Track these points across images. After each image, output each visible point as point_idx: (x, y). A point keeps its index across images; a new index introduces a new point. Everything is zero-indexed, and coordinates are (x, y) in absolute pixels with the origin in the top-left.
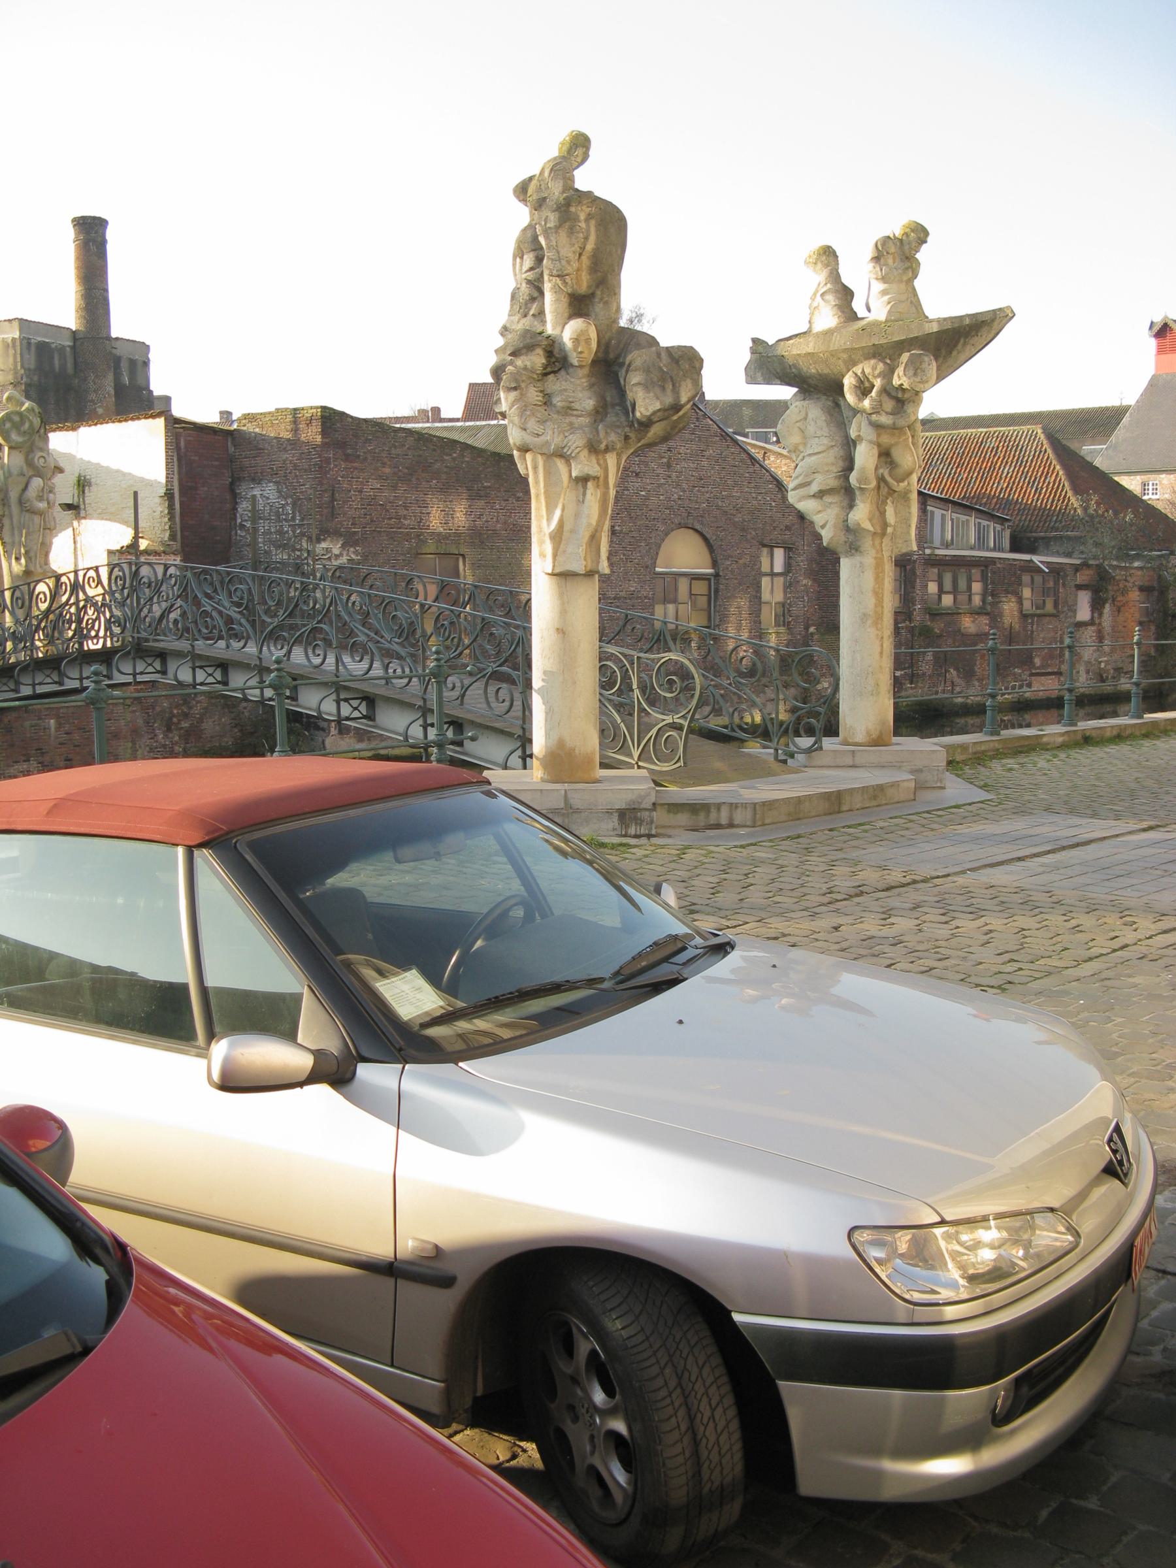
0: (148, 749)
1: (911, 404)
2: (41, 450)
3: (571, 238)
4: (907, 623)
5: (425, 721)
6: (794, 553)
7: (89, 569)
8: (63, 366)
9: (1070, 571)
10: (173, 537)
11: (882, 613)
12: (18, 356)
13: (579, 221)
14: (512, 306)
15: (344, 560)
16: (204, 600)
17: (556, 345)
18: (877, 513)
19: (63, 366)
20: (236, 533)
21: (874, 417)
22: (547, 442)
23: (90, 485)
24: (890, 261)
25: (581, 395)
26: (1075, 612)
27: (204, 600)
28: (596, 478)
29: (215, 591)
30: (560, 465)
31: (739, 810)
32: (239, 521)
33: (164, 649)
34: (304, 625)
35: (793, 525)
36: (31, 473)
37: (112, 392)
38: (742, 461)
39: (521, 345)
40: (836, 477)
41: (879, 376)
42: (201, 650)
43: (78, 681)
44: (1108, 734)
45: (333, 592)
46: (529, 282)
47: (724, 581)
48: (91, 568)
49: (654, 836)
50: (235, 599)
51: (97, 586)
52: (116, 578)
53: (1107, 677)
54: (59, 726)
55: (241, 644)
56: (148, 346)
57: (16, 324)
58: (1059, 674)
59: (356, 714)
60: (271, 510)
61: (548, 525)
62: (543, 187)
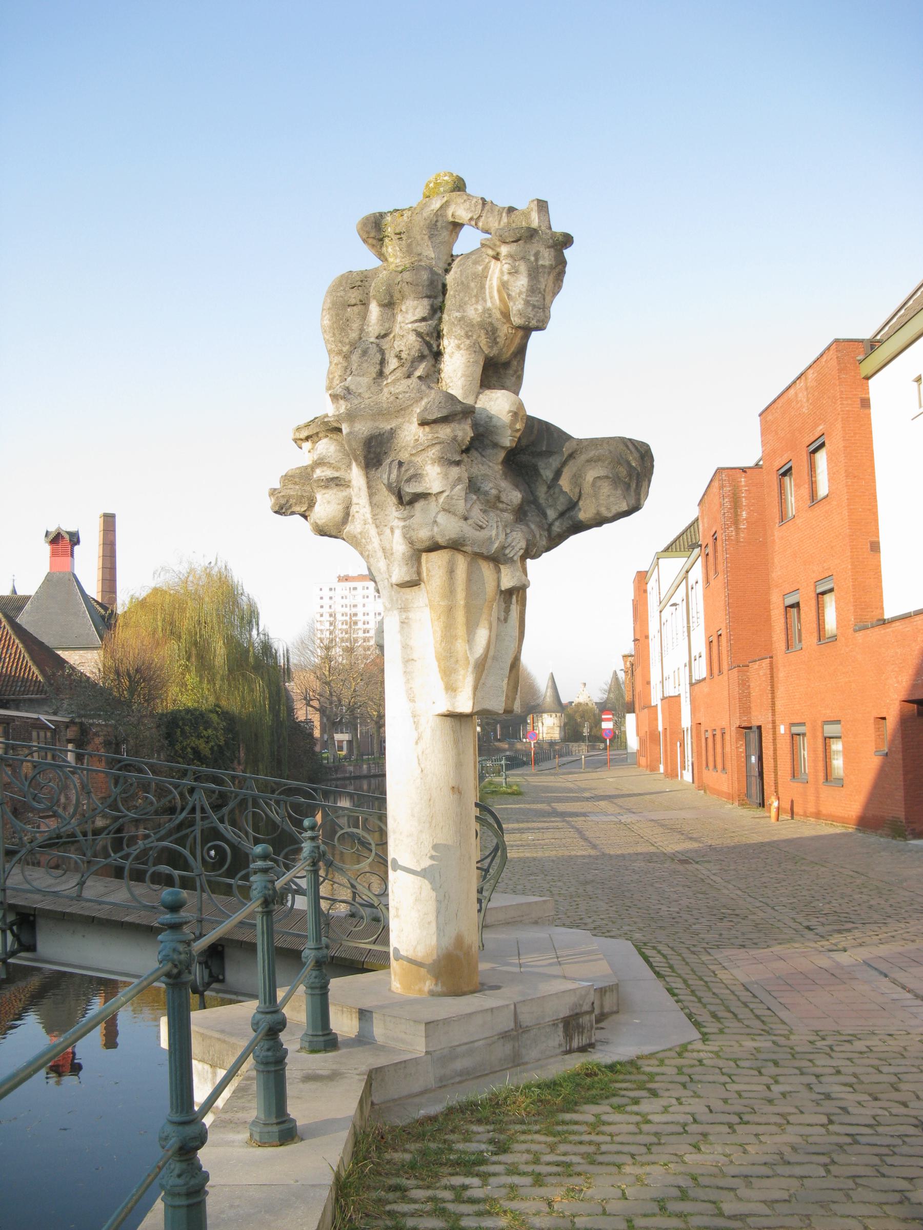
22: (490, 538)
30: (487, 569)
31: (608, 994)
46: (419, 334)
62: (439, 224)
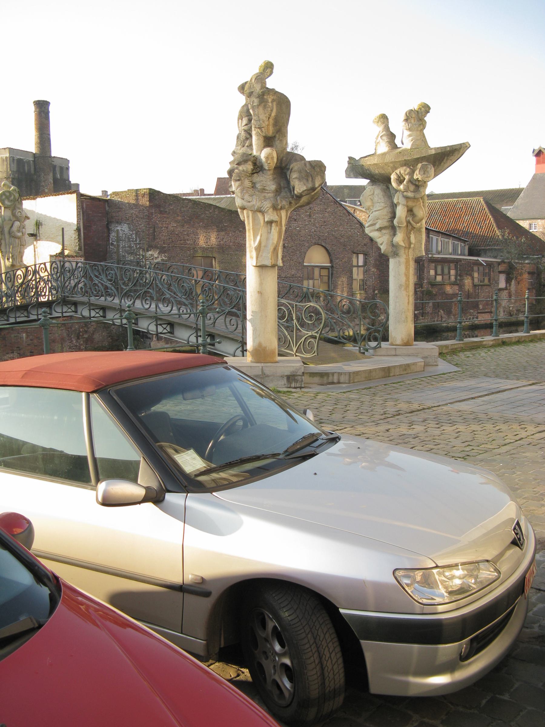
0: (68, 347)
1: (422, 187)
2: (19, 208)
3: (264, 110)
4: (421, 289)
5: (197, 334)
6: (368, 256)
7: (41, 264)
8: (29, 170)
9: (496, 265)
10: (80, 249)
11: (409, 284)
12: (9, 165)
13: (268, 103)
14: (237, 142)
15: (159, 260)
16: (95, 278)
17: (258, 160)
18: (407, 238)
19: (29, 170)
20: (109, 247)
21: (405, 193)
22: (254, 205)
23: (42, 225)
24: (413, 121)
25: (269, 183)
26: (498, 284)
27: (95, 278)
28: (276, 222)
29: (100, 274)
30: (260, 215)
31: (342, 376)
32: (111, 241)
33: (76, 301)
34: (141, 290)
35: (368, 243)
36: (14, 219)
37: (52, 182)
38: (344, 214)
39: (242, 160)
40: (387, 221)
41: (407, 174)
42: (93, 301)
43: (36, 316)
44: (514, 340)
45: (154, 274)
46: (245, 131)
47: (336, 270)
48: (42, 263)
49: (303, 388)
50: (109, 278)
51: (45, 272)
52: (54, 268)
53: (513, 314)
54: (27, 337)
55: (112, 298)
56: (69, 161)
57: (7, 150)
58: (491, 312)
59: (165, 331)
60: (125, 236)
61: (254, 243)
62: (251, 87)
